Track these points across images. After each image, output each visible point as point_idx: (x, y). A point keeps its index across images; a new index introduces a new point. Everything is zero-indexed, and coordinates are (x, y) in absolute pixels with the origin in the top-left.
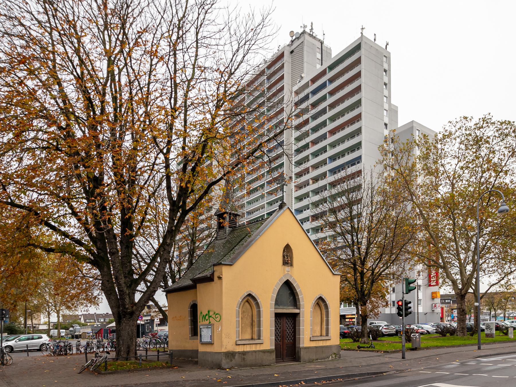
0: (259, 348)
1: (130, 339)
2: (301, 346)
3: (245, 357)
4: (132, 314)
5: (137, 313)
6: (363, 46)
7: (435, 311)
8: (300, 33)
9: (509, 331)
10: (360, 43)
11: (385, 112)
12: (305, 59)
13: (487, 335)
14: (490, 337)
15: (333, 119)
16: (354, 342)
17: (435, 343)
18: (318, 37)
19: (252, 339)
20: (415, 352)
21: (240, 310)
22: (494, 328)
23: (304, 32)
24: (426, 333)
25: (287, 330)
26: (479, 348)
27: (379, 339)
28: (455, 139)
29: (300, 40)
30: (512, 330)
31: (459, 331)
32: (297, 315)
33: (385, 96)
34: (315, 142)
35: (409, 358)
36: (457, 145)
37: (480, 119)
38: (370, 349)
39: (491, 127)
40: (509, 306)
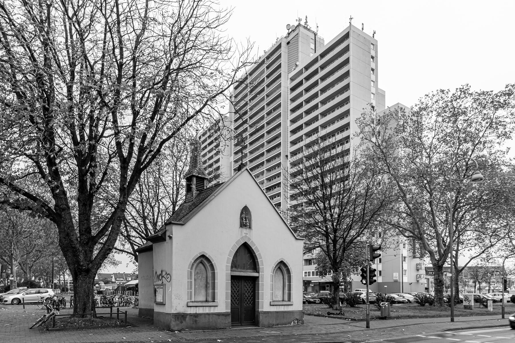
0: (212, 310)
1: (87, 297)
2: (260, 310)
3: (197, 319)
4: (88, 271)
5: (94, 271)
6: (351, 34)
7: (420, 282)
8: (296, 26)
9: (489, 304)
10: (349, 32)
11: (372, 95)
12: (300, 49)
13: (466, 307)
14: (468, 309)
15: (324, 102)
16: (330, 308)
17: (411, 313)
18: (312, 29)
19: (207, 301)
20: (384, 321)
21: (193, 271)
22: (473, 300)
23: (299, 25)
24: (407, 302)
25: (246, 294)
26: (452, 320)
27: (356, 306)
28: (432, 112)
29: (295, 33)
30: (492, 304)
31: (437, 301)
32: (257, 278)
33: (372, 81)
34: (308, 124)
35: (373, 328)
36: (434, 118)
37: (457, 89)
38: (340, 316)
39: (469, 97)
40: (494, 280)
